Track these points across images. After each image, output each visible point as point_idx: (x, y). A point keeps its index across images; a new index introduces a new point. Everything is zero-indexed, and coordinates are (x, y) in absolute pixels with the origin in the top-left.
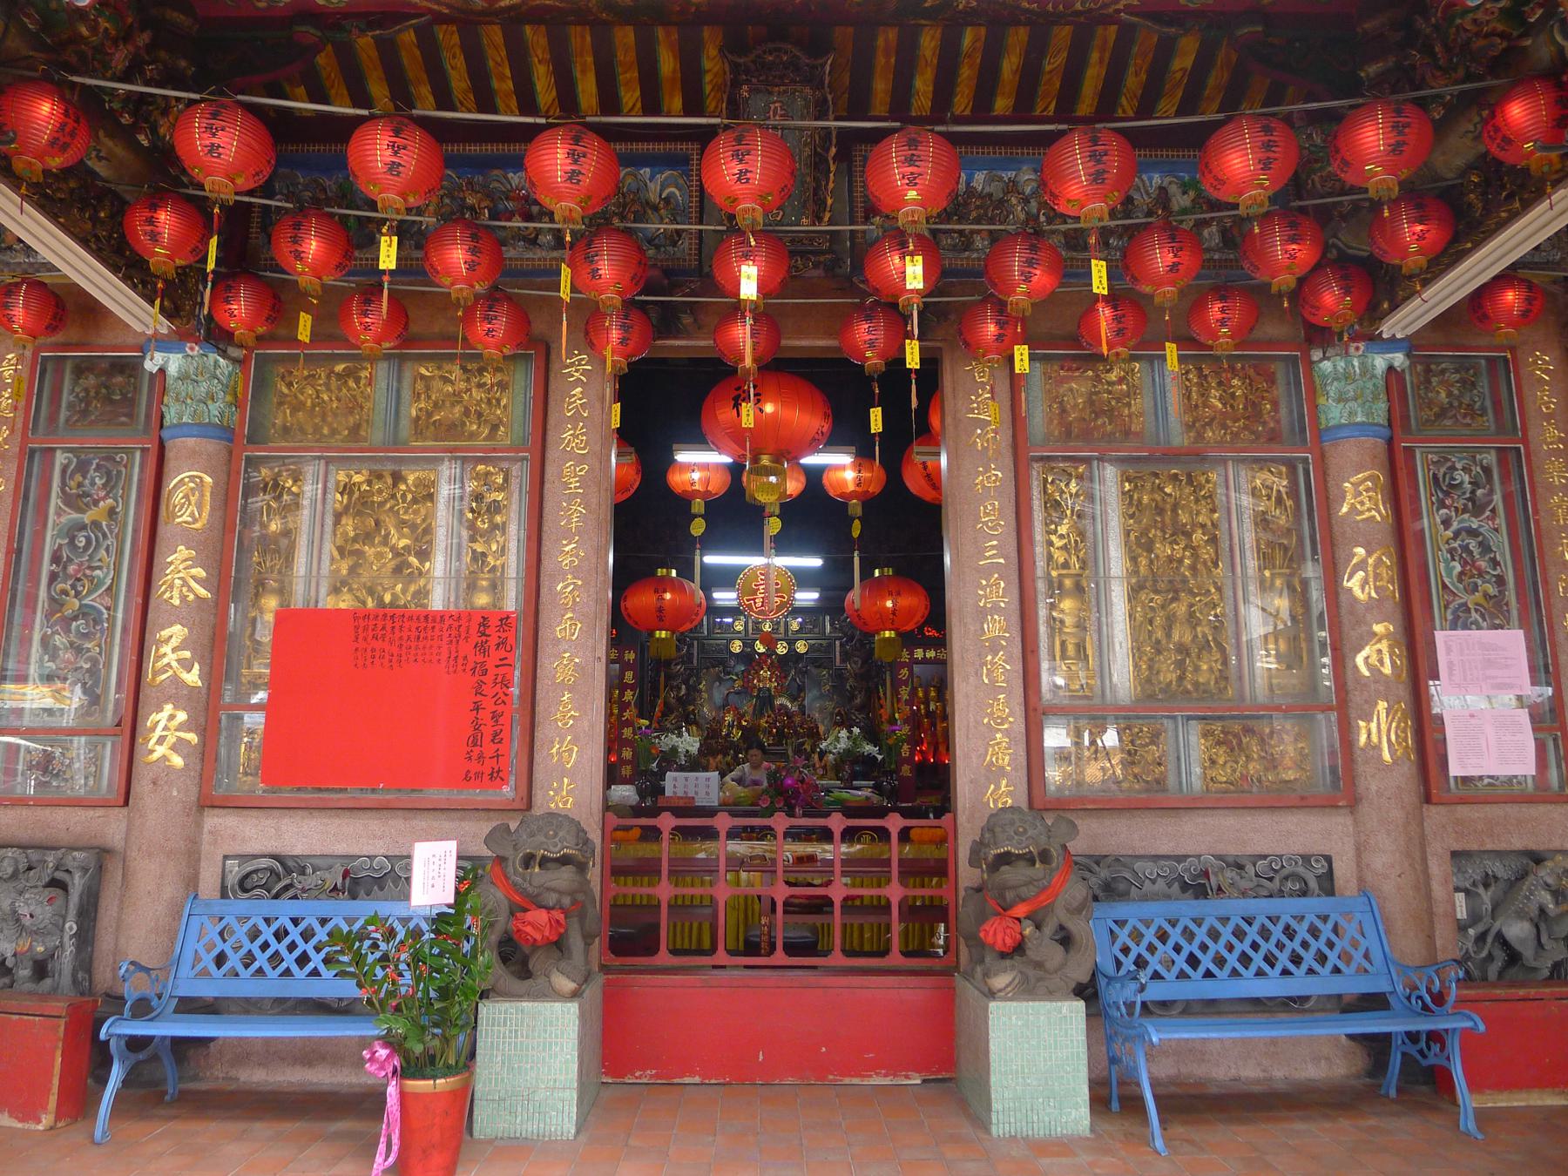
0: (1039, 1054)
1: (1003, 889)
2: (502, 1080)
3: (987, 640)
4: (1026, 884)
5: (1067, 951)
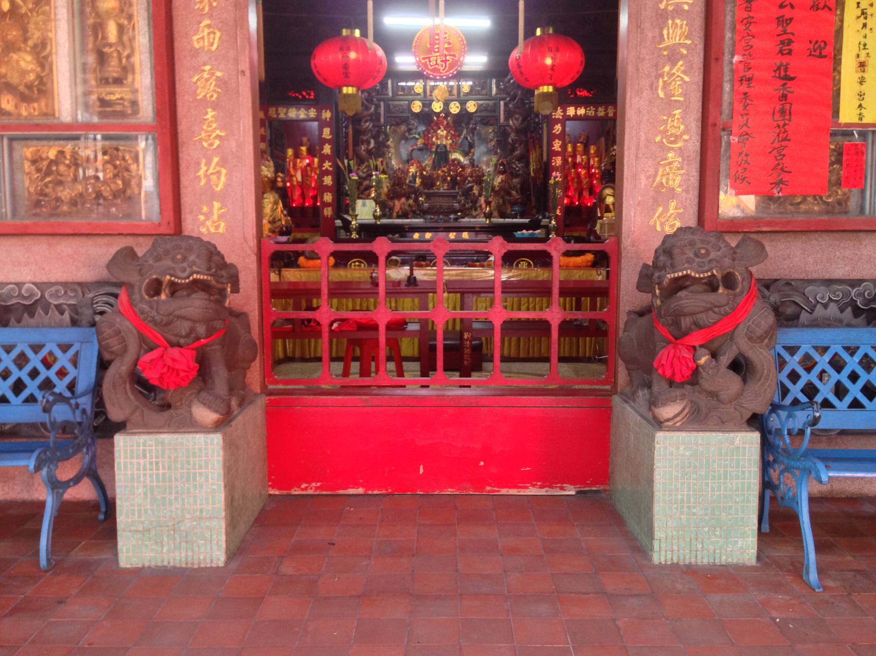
0: (707, 484)
1: (677, 316)
2: (146, 510)
3: (665, 49)
4: (707, 310)
5: (745, 380)
